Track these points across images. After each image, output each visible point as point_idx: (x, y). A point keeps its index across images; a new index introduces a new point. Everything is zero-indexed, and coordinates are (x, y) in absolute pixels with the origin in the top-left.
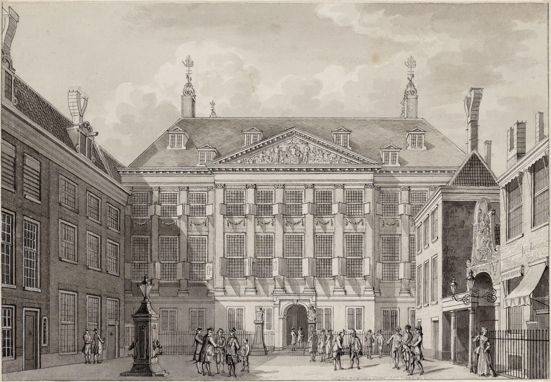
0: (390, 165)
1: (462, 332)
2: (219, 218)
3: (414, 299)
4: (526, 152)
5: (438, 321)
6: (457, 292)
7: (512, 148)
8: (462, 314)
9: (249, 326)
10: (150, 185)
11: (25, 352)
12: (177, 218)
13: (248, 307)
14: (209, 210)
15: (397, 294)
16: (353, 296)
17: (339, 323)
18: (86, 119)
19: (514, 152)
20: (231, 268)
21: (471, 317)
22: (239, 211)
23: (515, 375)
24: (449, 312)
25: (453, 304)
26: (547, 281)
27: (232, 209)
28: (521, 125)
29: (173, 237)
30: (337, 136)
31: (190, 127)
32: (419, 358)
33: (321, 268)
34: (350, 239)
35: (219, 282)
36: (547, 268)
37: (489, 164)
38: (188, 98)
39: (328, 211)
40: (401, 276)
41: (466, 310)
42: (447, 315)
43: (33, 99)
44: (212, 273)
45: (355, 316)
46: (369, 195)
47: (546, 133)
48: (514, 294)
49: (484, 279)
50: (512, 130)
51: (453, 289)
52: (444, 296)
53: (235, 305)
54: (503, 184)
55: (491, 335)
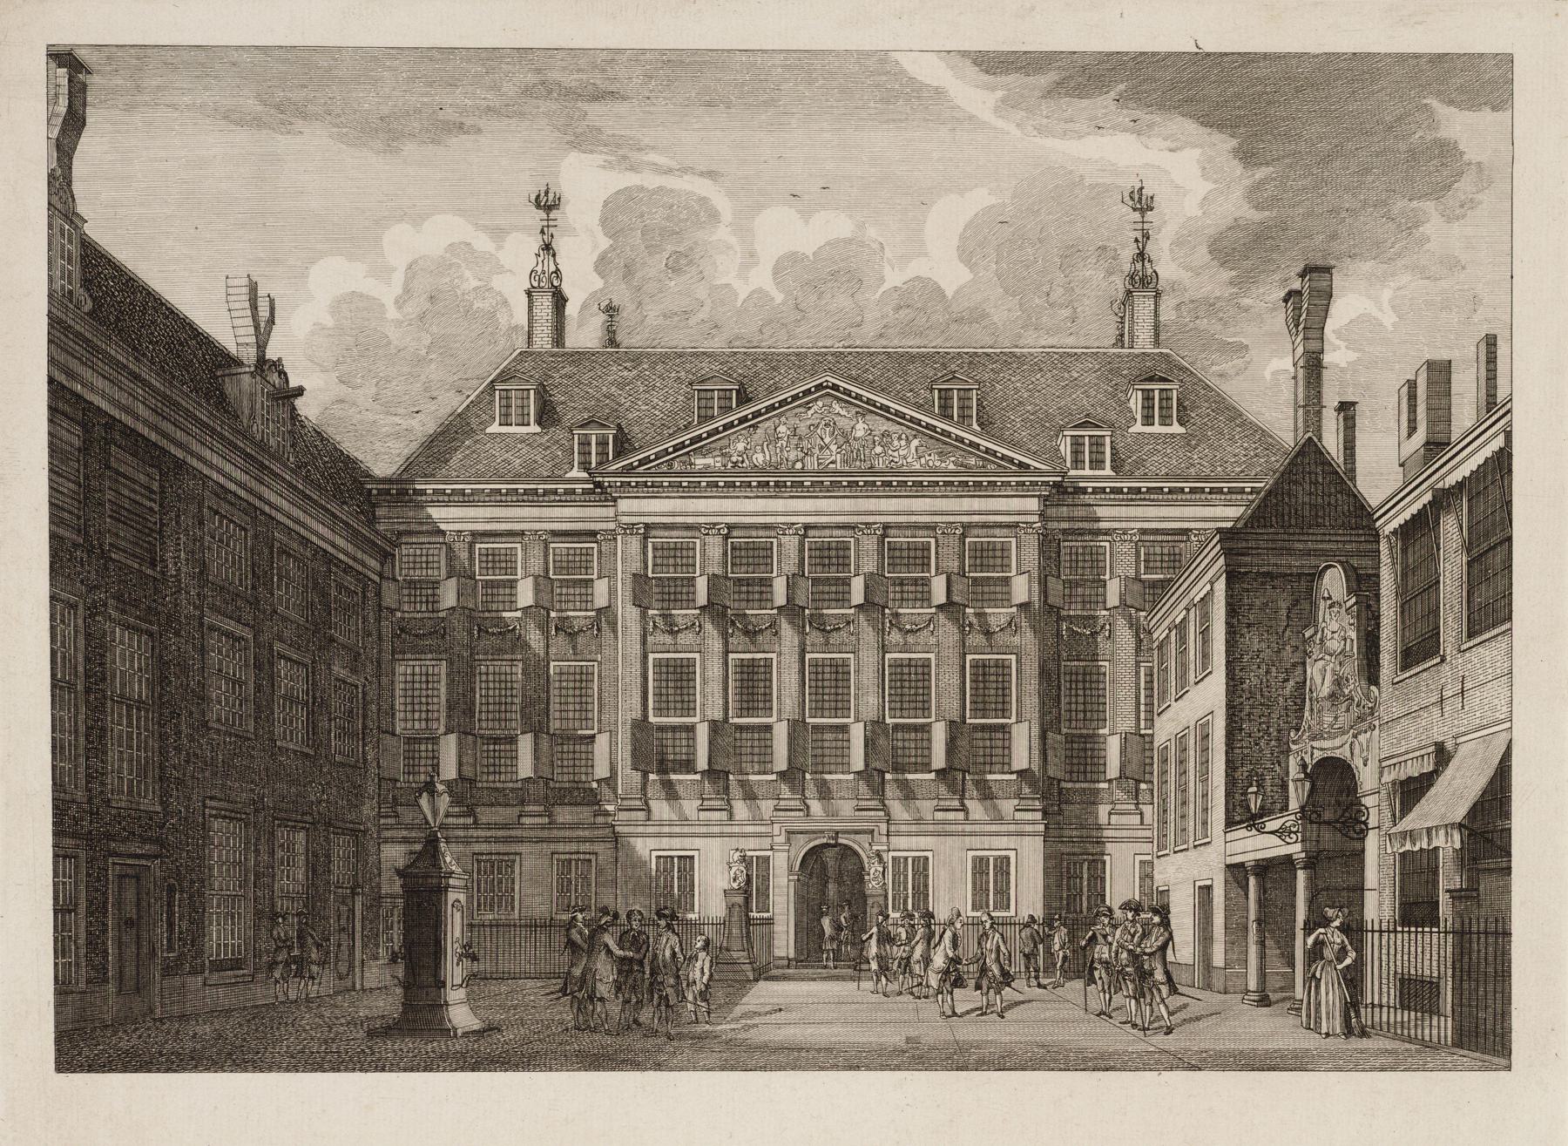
0: (1087, 472)
1: (1274, 922)
2: (628, 614)
7: (1412, 429)
8: (1271, 871)
11: (599, 563)
13: (712, 851)
17: (951, 896)
18: (271, 354)
19: (1420, 436)
21: (1301, 876)
22: (678, 591)
23: (1435, 1039)
27: (659, 591)
28: (1440, 372)
29: (443, 699)
31: (541, 384)
34: (920, 684)
35: (628, 778)
36: (1509, 747)
38: (545, 305)
39: (999, 554)
40: (458, 915)
41: (1288, 860)
42: (1236, 872)
44: (609, 754)
45: (991, 877)
46: (1024, 557)
47: (1501, 395)
48: (1414, 820)
49: (1334, 777)
50: (1412, 385)
52: (1230, 823)
53: (676, 846)
54: (1390, 525)
55: (1355, 930)
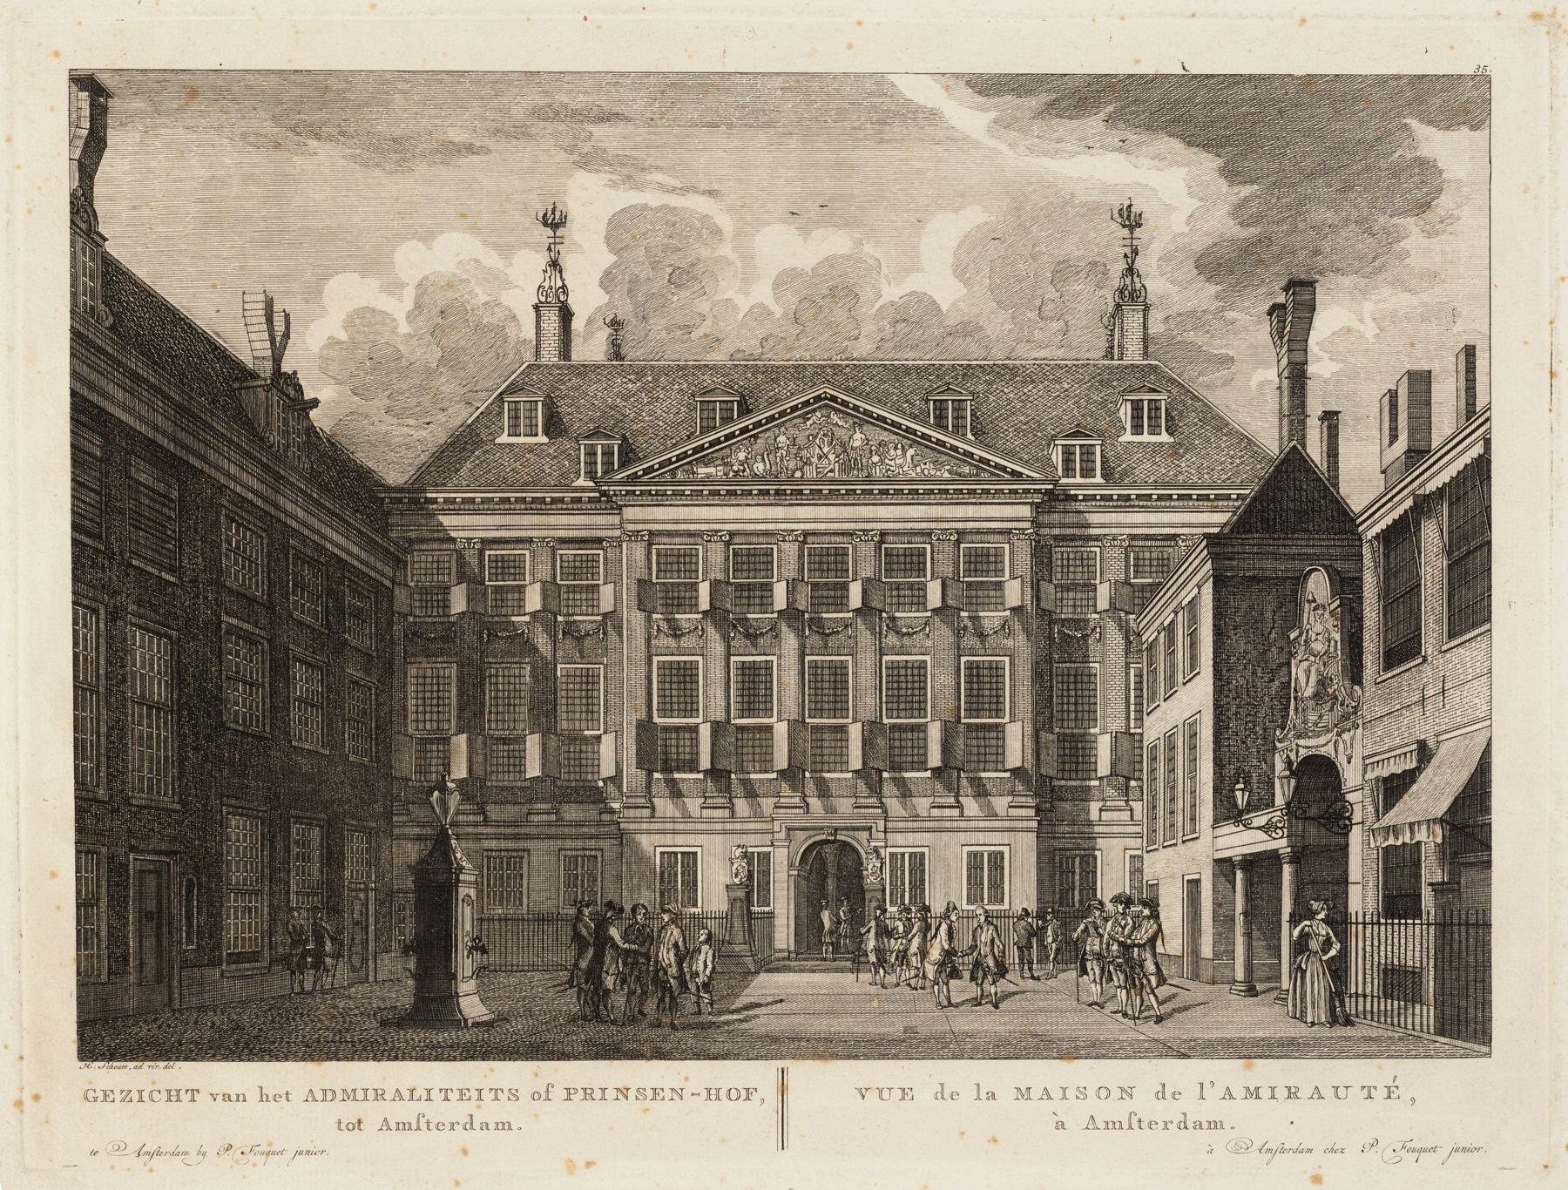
1: (1261, 917)
2: (634, 619)
3: (1138, 829)
4: (1436, 442)
5: (1197, 882)
6: (1251, 807)
8: (1259, 867)
9: (714, 891)
10: (453, 534)
12: (527, 618)
14: (606, 596)
15: (1094, 815)
16: (977, 819)
17: (947, 888)
20: (660, 754)
24: (1229, 860)
25: (1241, 841)
26: (1489, 764)
28: (1420, 382)
30: (947, 402)
32: (1153, 980)
33: (891, 754)
36: (1489, 745)
37: (1336, 486)
38: (551, 321)
41: (1274, 855)
42: (1224, 867)
43: (274, 80)
45: (986, 872)
49: (1318, 775)
50: (1393, 395)
51: (1241, 798)
55: (1339, 922)
